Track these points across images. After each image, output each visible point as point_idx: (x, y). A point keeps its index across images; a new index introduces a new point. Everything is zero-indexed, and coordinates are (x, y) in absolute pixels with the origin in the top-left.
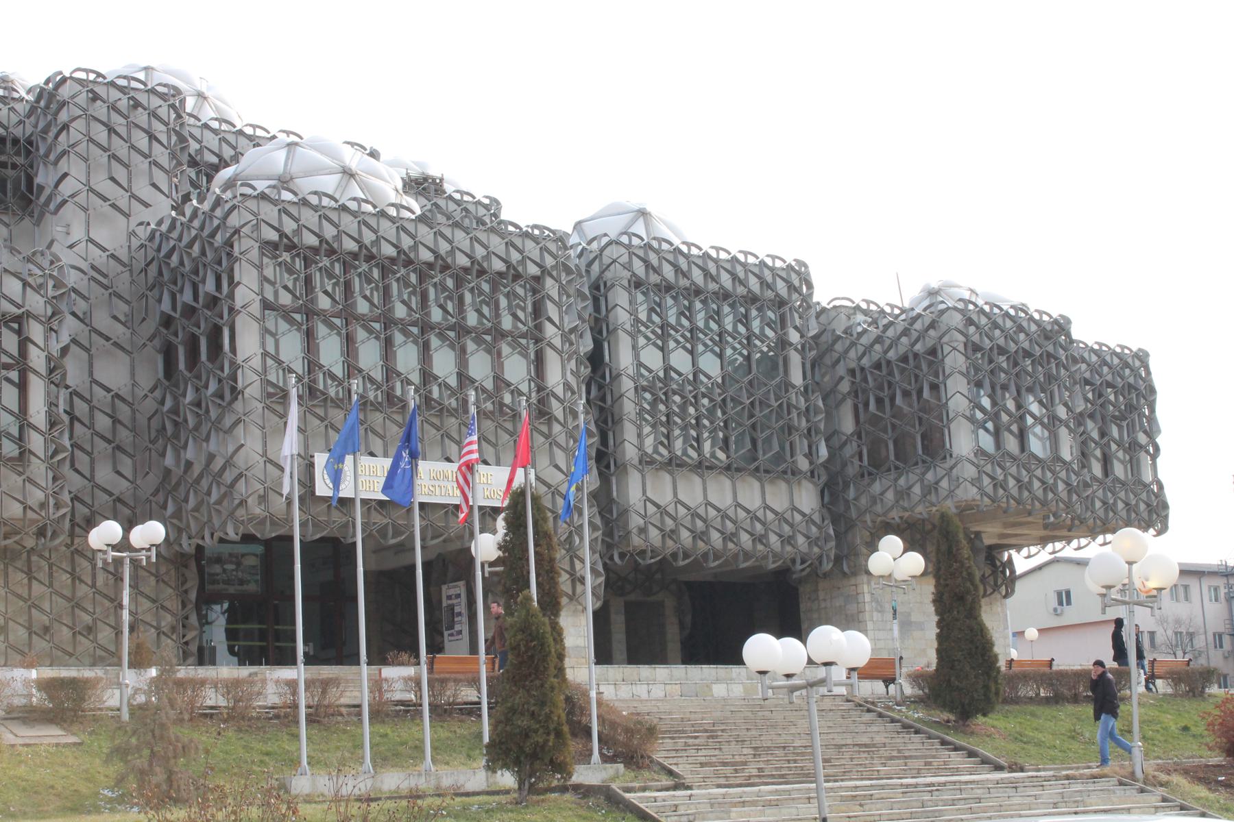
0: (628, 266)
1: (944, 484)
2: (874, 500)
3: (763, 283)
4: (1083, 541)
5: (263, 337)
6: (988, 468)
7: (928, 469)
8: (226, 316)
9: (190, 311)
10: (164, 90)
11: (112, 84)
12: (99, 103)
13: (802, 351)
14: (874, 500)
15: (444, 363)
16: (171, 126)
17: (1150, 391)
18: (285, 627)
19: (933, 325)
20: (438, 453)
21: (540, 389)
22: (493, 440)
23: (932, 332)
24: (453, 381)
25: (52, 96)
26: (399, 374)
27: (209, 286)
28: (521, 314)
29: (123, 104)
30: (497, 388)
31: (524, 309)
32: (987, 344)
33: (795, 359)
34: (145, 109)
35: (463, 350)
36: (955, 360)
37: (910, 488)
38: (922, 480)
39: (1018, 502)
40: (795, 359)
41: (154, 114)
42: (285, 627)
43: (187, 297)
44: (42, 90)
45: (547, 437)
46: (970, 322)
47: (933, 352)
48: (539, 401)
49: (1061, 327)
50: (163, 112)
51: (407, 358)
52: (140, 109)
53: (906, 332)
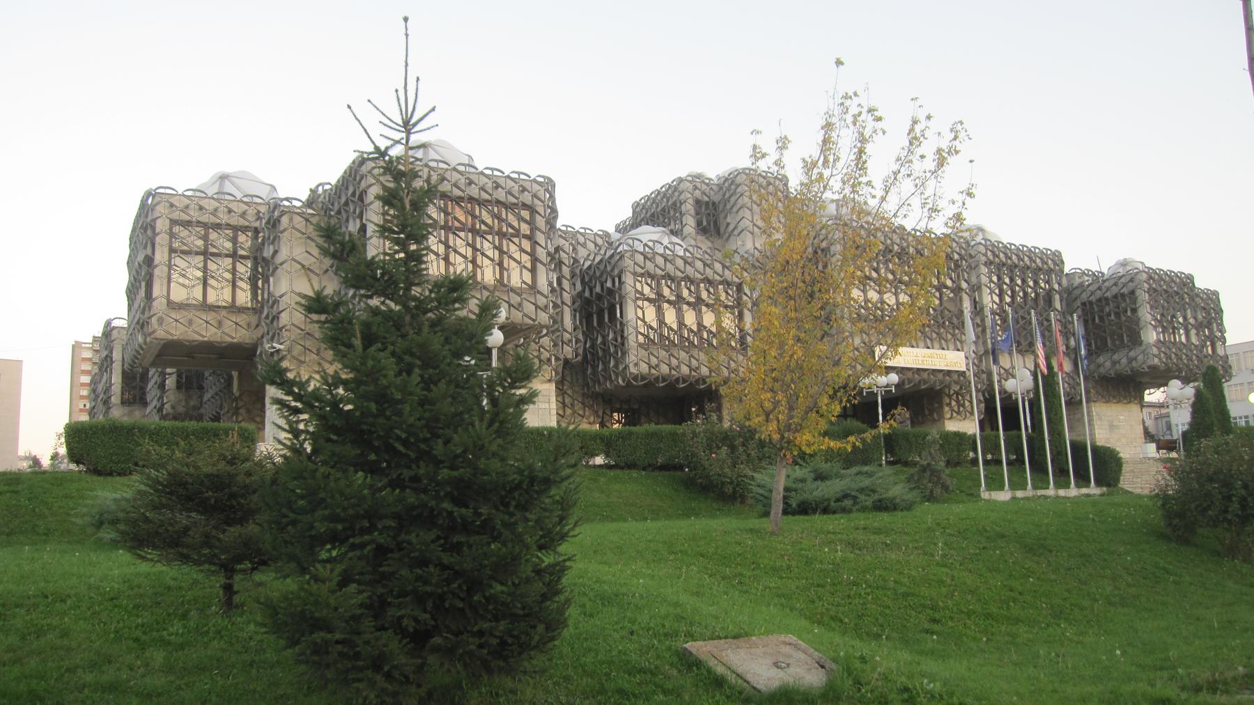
0: (985, 255)
1: (1140, 357)
2: (1099, 366)
3: (1020, 259)
4: (1152, 391)
5: (636, 309)
6: (1163, 349)
7: (1115, 353)
8: (617, 299)
9: (599, 297)
10: (542, 180)
11: (535, 181)
12: (526, 193)
13: (1059, 293)
14: (1099, 366)
15: (690, 318)
16: (546, 203)
17: (1219, 311)
18: (880, 401)
19: (1132, 280)
20: (908, 344)
21: (741, 330)
22: (697, 357)
23: (1130, 284)
24: (695, 328)
25: (676, 189)
26: (686, 326)
27: (609, 284)
28: (730, 292)
29: (516, 188)
30: (699, 330)
31: (732, 289)
32: (1159, 289)
33: (1057, 297)
34: (529, 192)
35: (700, 311)
36: (1143, 296)
37: (1137, 356)
38: (1127, 356)
39: (1176, 365)
40: (1057, 297)
41: (535, 196)
42: (880, 401)
43: (598, 289)
44: (670, 186)
45: (937, 334)
46: (1151, 278)
47: (1133, 292)
48: (741, 337)
49: (1190, 278)
50: (541, 194)
51: (670, 317)
52: (526, 193)
53: (1115, 285)
